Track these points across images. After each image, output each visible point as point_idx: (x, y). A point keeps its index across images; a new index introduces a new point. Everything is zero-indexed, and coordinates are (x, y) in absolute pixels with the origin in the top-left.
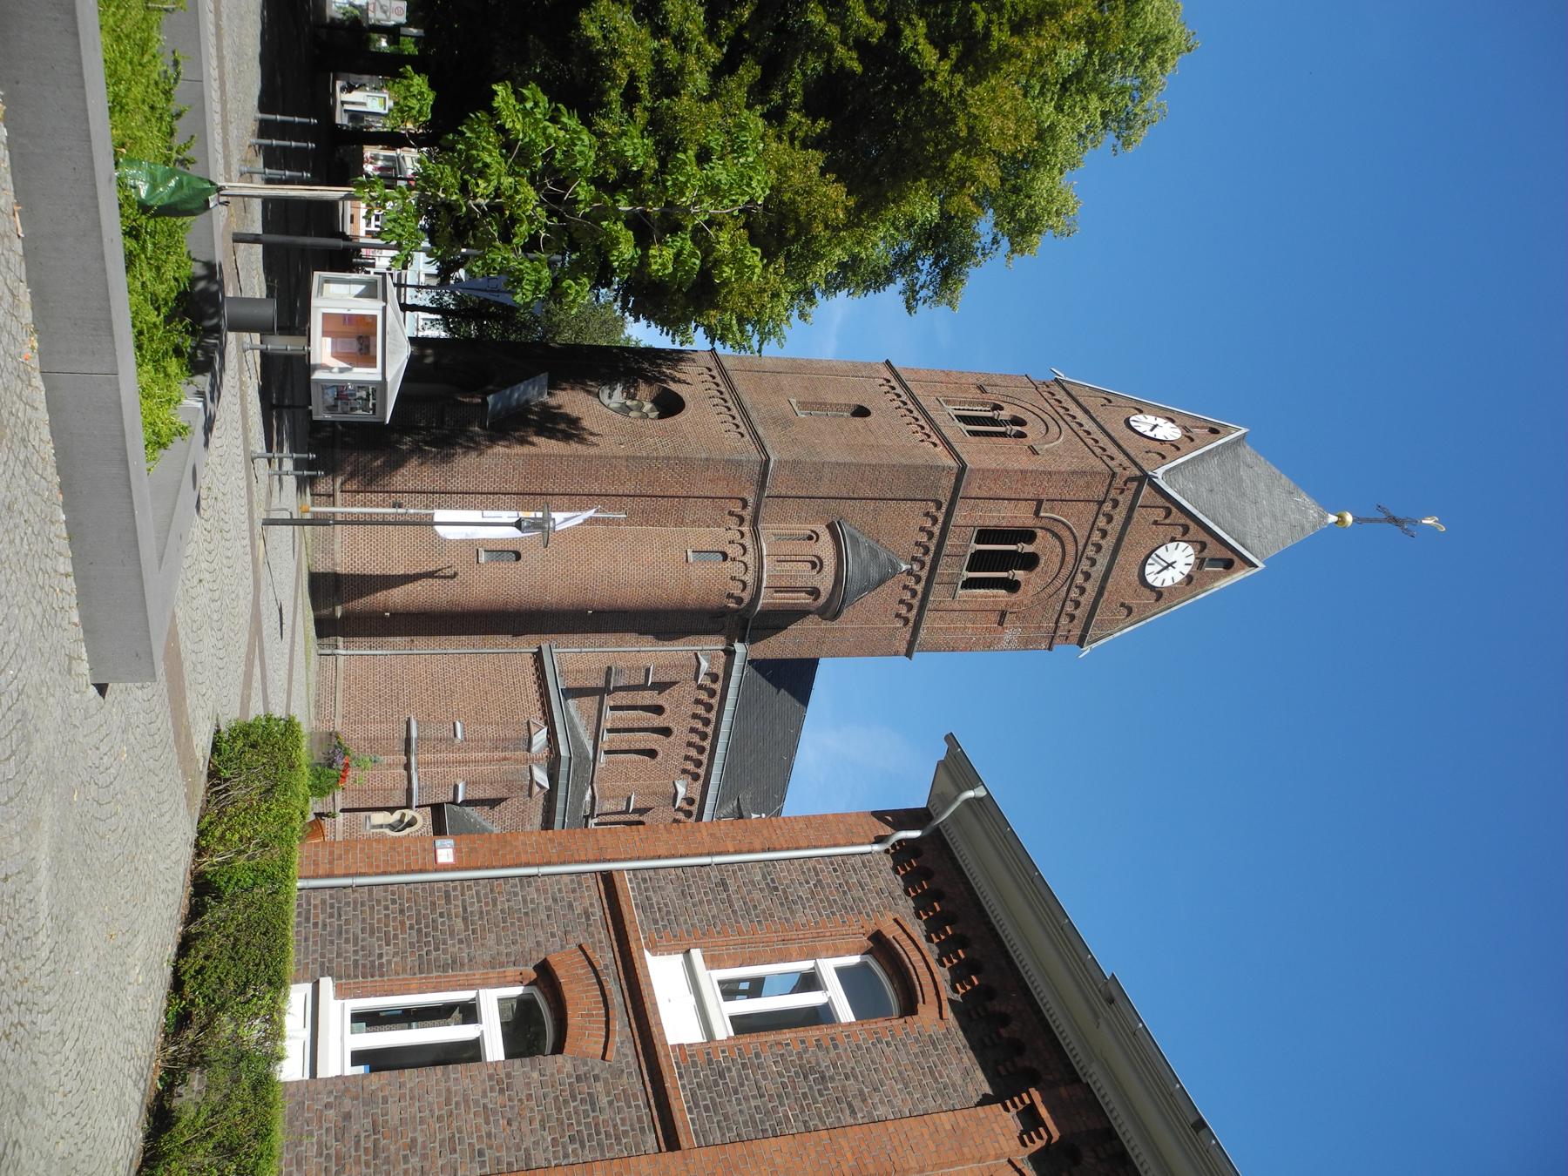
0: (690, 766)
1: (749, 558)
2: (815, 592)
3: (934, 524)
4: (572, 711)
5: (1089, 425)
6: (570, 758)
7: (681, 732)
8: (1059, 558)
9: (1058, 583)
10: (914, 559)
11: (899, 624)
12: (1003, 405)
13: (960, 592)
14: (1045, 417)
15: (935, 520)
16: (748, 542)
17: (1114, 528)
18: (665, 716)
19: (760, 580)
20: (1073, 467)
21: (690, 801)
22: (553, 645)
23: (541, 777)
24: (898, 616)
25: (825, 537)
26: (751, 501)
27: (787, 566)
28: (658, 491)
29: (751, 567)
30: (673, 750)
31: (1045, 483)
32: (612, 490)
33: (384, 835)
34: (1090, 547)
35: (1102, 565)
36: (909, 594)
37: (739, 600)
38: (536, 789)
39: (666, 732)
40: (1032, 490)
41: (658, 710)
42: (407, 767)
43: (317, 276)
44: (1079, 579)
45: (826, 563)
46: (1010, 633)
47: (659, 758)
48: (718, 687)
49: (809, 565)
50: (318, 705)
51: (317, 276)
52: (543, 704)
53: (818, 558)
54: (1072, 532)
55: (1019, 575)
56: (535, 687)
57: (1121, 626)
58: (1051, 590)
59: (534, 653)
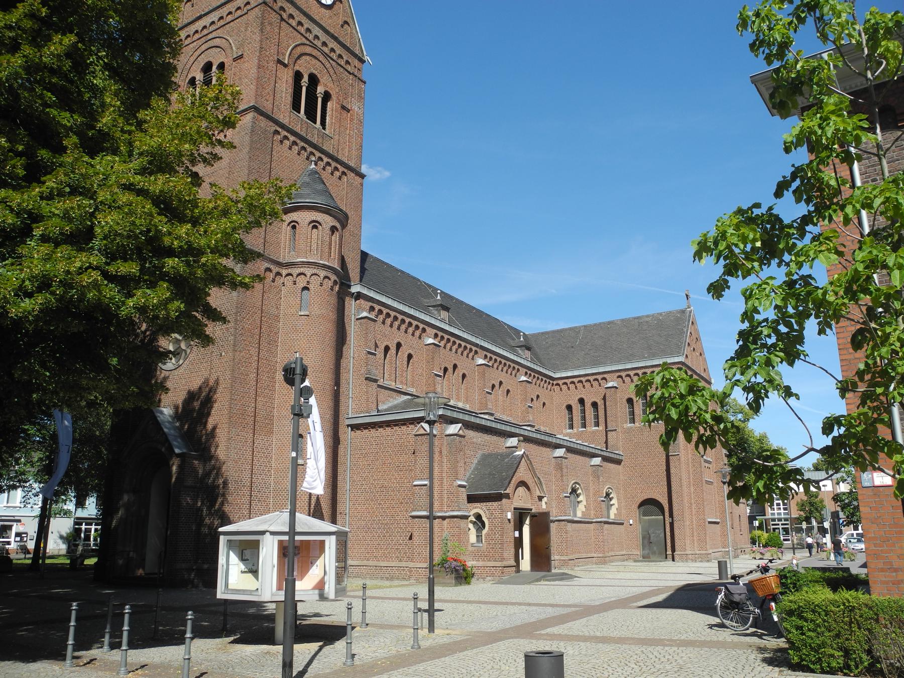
0: (418, 333)
1: (309, 271)
2: (333, 229)
3: (288, 139)
4: (385, 407)
5: (214, 17)
6: (444, 408)
7: (399, 336)
8: (313, 59)
9: (326, 63)
10: (308, 158)
11: (345, 178)
12: (190, 76)
13: (327, 132)
14: (204, 47)
15: (286, 138)
16: (295, 271)
17: (299, 17)
18: (390, 346)
19: (324, 267)
20: (257, 31)
21: (436, 336)
22: (346, 416)
23: (453, 429)
24: (340, 178)
25: (294, 216)
26: (267, 265)
27: (314, 246)
28: (257, 331)
29: (315, 271)
30: (410, 343)
31: (267, 53)
32: (254, 365)
33: (487, 535)
34: (307, 35)
35: (318, 31)
36: (328, 167)
37: (335, 282)
38: (461, 432)
39: (399, 345)
40: (271, 64)
41: (387, 349)
42: (444, 518)
43: (220, 595)
44: (326, 50)
45: (314, 218)
46: (355, 107)
47: (412, 353)
48: (377, 307)
49: (315, 230)
50: (391, 579)
51: (220, 595)
52: (395, 425)
53: (310, 223)
54: (299, 45)
55: (320, 89)
56: (381, 430)
57: (354, 31)
58: (331, 70)
59: (352, 430)
